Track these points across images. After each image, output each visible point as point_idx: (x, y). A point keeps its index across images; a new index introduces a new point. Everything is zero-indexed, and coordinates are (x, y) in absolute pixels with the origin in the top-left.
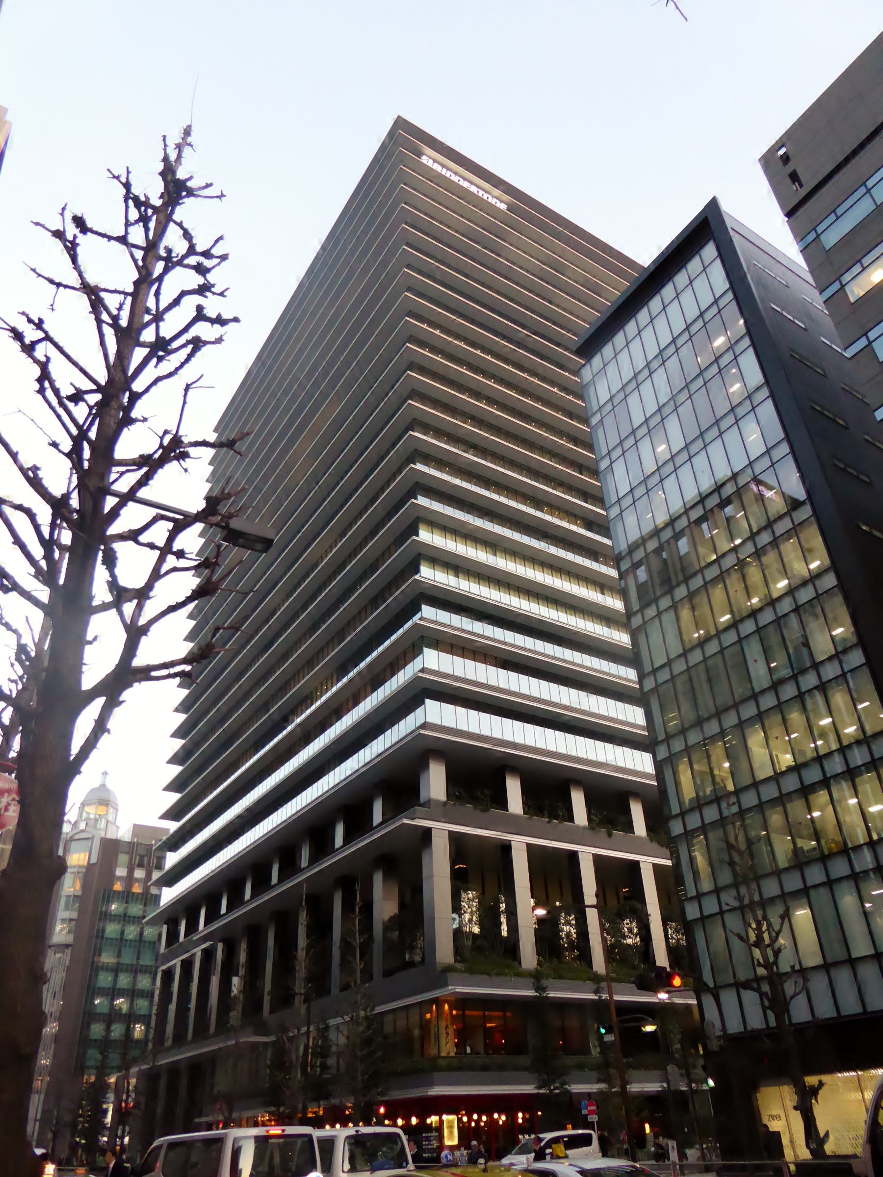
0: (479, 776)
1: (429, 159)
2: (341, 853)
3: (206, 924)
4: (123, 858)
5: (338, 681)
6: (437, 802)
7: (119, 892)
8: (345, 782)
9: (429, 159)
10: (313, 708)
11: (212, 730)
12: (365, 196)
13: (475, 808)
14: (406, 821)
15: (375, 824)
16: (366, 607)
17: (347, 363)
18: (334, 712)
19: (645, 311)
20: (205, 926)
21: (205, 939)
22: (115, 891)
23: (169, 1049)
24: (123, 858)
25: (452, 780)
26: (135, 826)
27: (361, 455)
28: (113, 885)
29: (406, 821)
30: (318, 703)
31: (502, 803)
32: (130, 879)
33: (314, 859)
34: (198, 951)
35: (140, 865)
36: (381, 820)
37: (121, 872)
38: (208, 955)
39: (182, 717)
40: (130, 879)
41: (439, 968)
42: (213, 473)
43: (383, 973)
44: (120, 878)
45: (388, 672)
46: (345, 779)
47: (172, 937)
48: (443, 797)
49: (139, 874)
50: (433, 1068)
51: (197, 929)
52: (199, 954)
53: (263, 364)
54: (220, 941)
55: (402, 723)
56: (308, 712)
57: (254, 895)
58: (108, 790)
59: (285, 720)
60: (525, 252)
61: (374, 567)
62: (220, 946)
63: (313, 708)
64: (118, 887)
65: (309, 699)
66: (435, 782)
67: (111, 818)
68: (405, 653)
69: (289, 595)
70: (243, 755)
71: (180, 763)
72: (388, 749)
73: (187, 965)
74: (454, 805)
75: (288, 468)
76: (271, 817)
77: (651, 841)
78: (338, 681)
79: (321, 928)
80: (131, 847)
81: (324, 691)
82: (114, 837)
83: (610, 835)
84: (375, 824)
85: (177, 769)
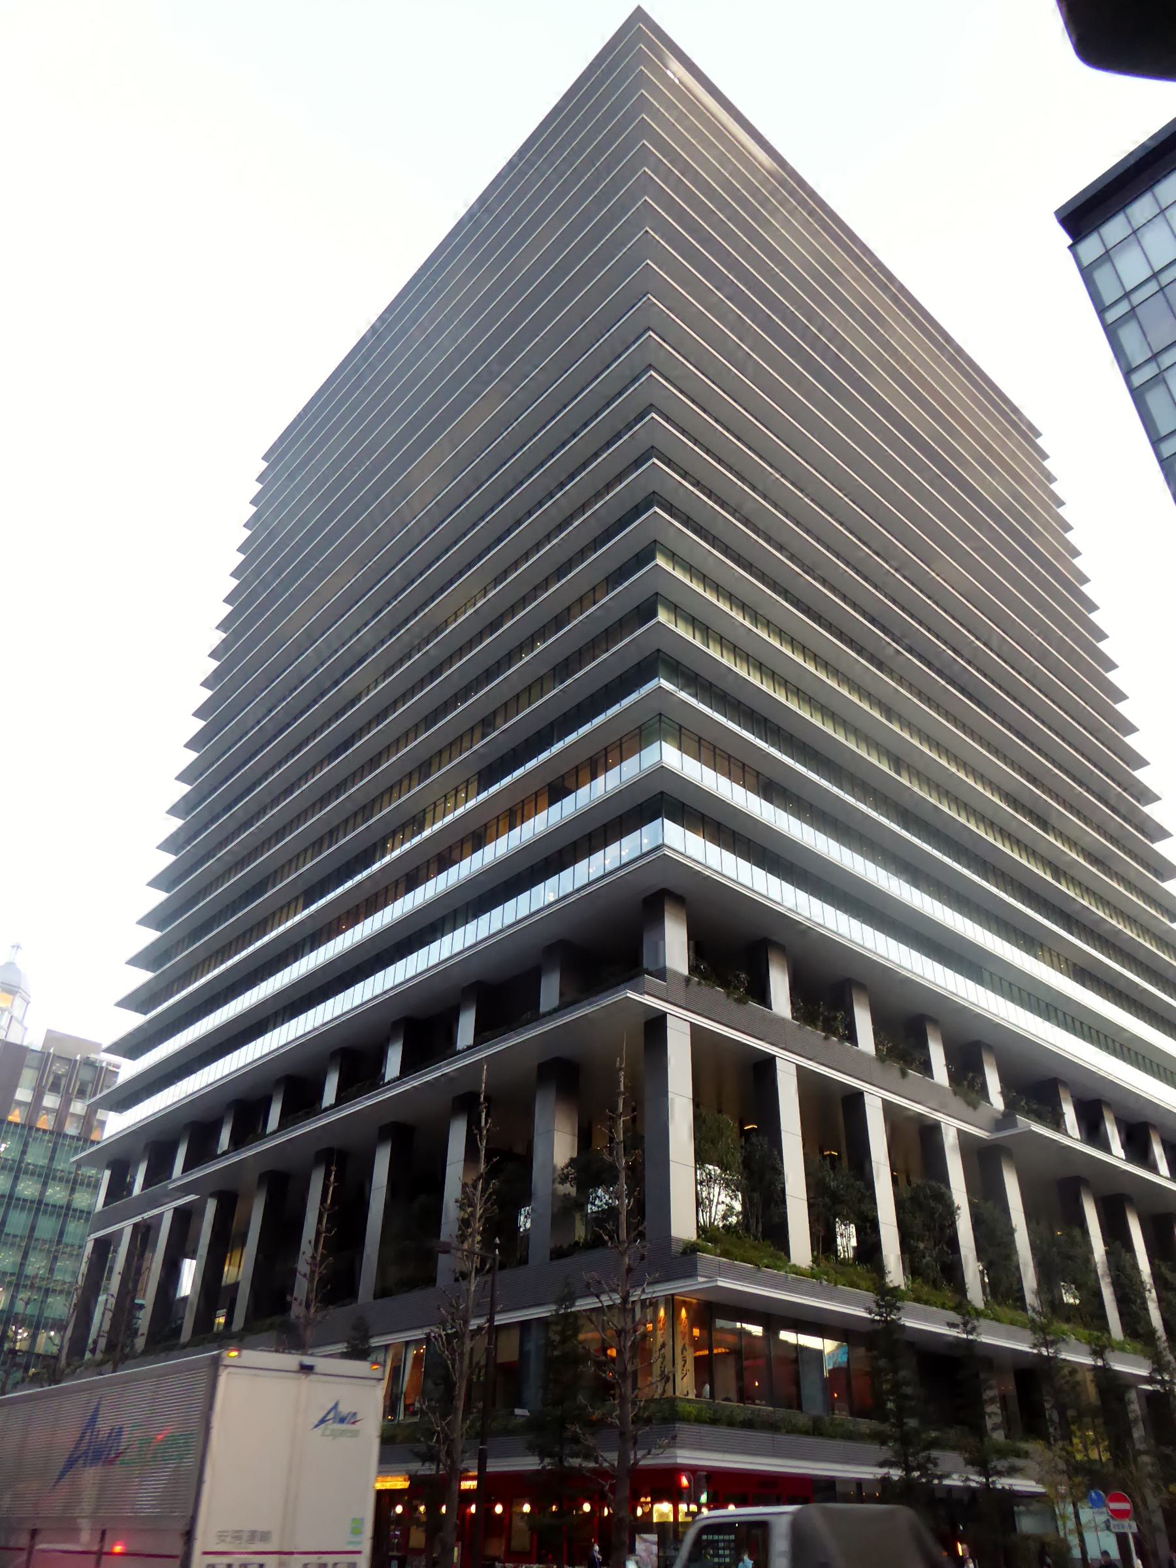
0: (736, 949)
1: (675, 70)
2: (472, 1054)
3: (186, 1168)
4: (28, 1076)
5: (305, 907)
6: (676, 974)
7: (16, 1125)
8: (391, 994)
9: (675, 70)
10: (266, 939)
11: (405, 738)
12: (432, 279)
13: (728, 995)
14: (631, 995)
15: (219, 1152)
16: (410, 774)
17: (364, 504)
18: (475, 836)
19: (1120, 220)
20: (183, 1171)
21: (185, 1189)
22: (10, 1123)
23: (184, 1346)
24: (28, 1076)
25: (698, 947)
26: (49, 1031)
27: (492, 510)
28: (8, 1112)
29: (631, 995)
30: (274, 934)
31: (763, 997)
32: (35, 1106)
33: (237, 1142)
34: (167, 1212)
35: (55, 1088)
36: (333, 1101)
37: (23, 1094)
38: (185, 1219)
39: (169, 859)
40: (35, 1106)
41: (676, 1249)
42: (256, 517)
43: (552, 1252)
44: (20, 1104)
45: (434, 867)
46: (392, 989)
47: (119, 1188)
48: (685, 971)
49: (50, 1101)
50: (667, 1417)
51: (170, 1177)
52: (128, 1232)
53: (477, 225)
54: (212, 1195)
55: (400, 965)
56: (259, 944)
57: (286, 1121)
58: (18, 972)
59: (365, 859)
60: (789, 235)
61: (558, 622)
62: (211, 1206)
63: (266, 939)
64: (16, 1116)
65: (417, 823)
66: (675, 946)
67: (17, 1013)
68: (620, 744)
69: (386, 674)
70: (394, 834)
71: (158, 928)
72: (456, 955)
73: (144, 1234)
74: (699, 983)
75: (403, 490)
76: (229, 1057)
77: (955, 1093)
78: (304, 908)
79: (418, 1179)
80: (44, 1059)
81: (396, 843)
82: (18, 1042)
83: (904, 1074)
84: (219, 1152)
85: (152, 935)
